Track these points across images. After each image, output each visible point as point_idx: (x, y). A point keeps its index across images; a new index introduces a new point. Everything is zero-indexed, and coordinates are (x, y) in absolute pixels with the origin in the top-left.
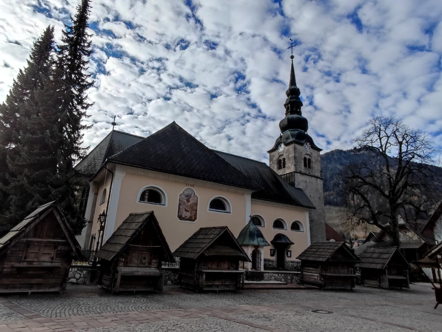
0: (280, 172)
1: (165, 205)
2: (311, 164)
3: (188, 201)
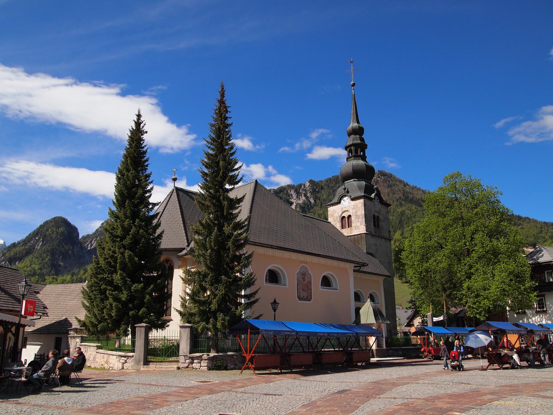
0: (346, 232)
2: (380, 223)
3: (304, 280)
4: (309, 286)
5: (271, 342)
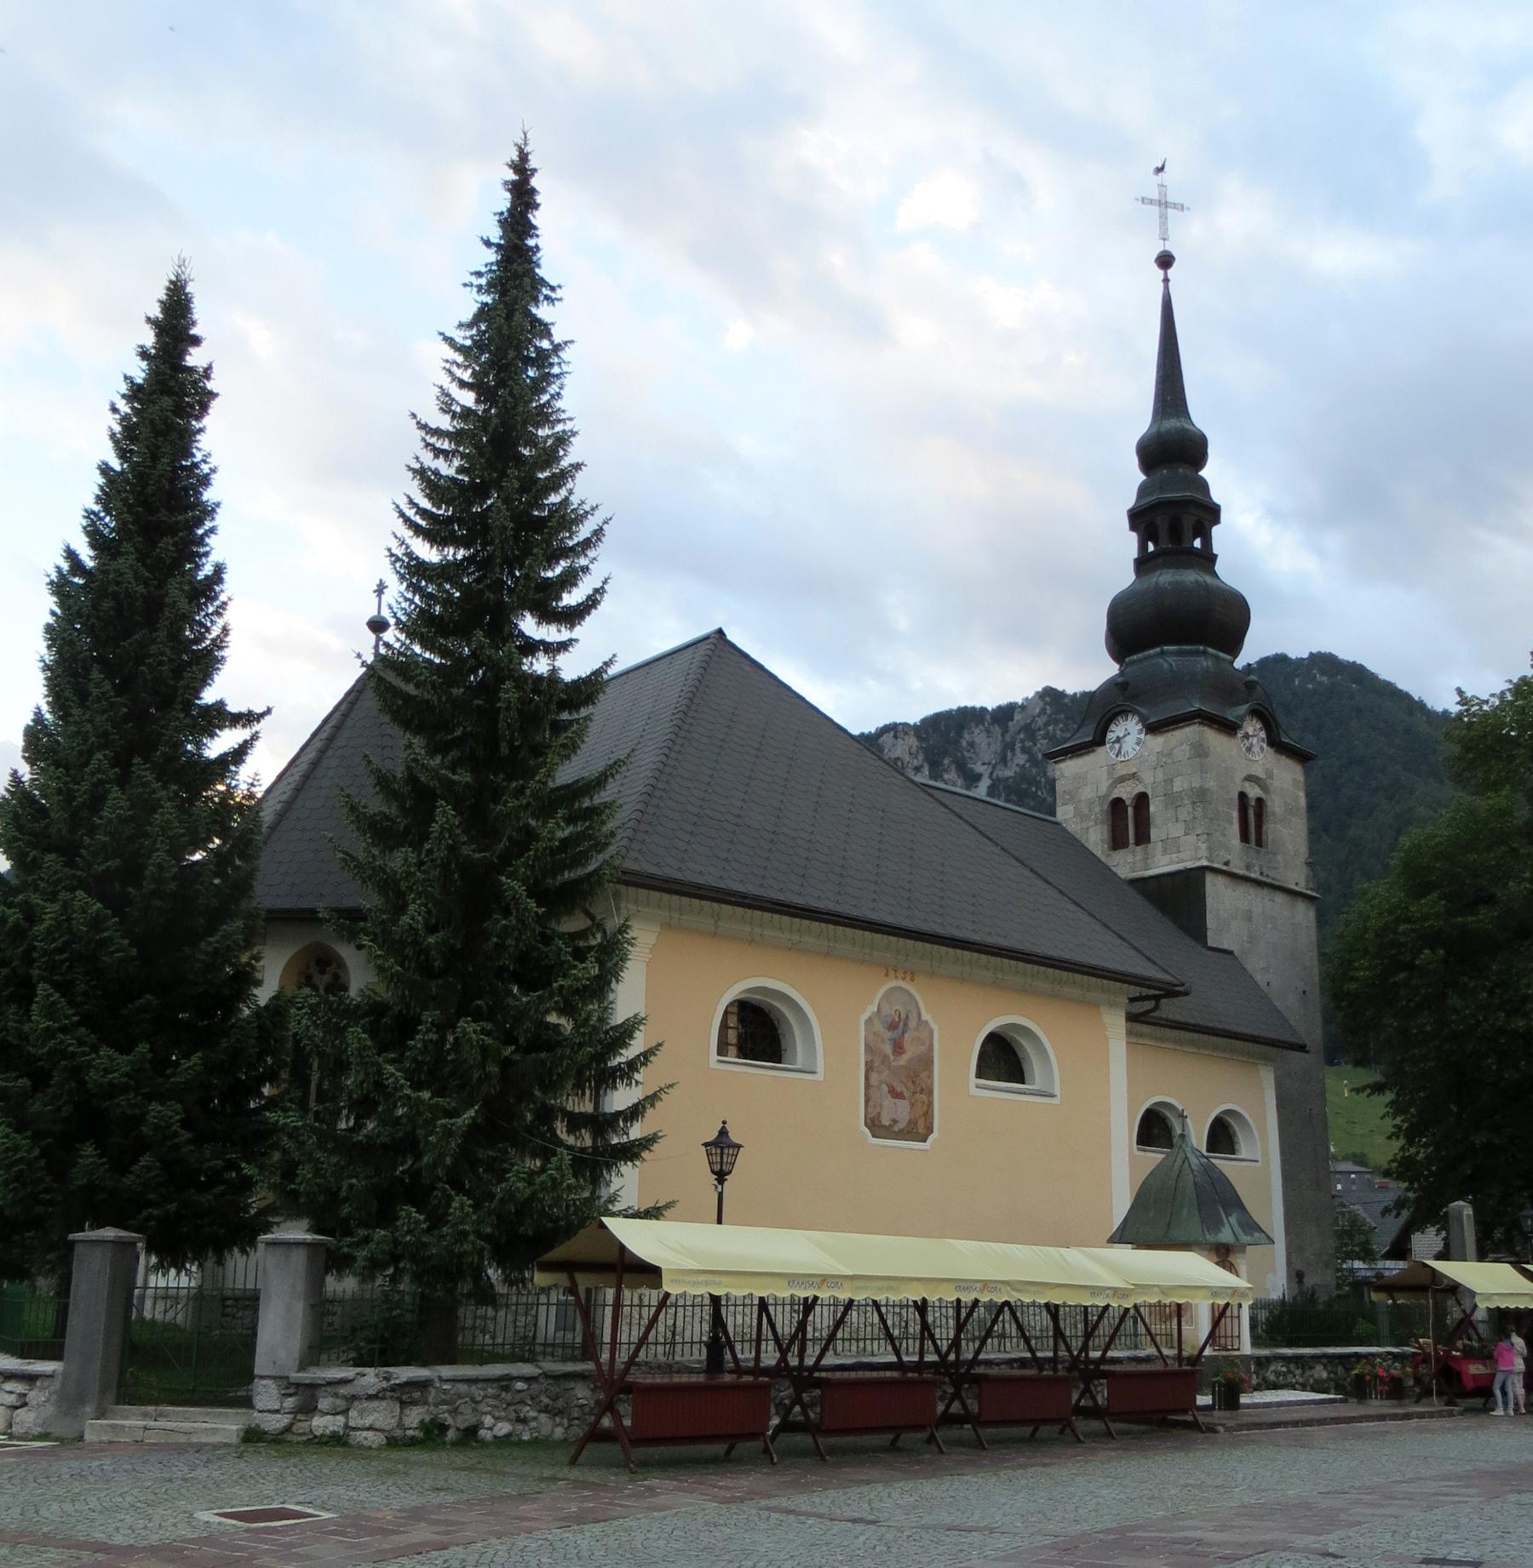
1: (814, 1073)
3: (898, 1048)
4: (924, 1075)
5: (739, 1318)
